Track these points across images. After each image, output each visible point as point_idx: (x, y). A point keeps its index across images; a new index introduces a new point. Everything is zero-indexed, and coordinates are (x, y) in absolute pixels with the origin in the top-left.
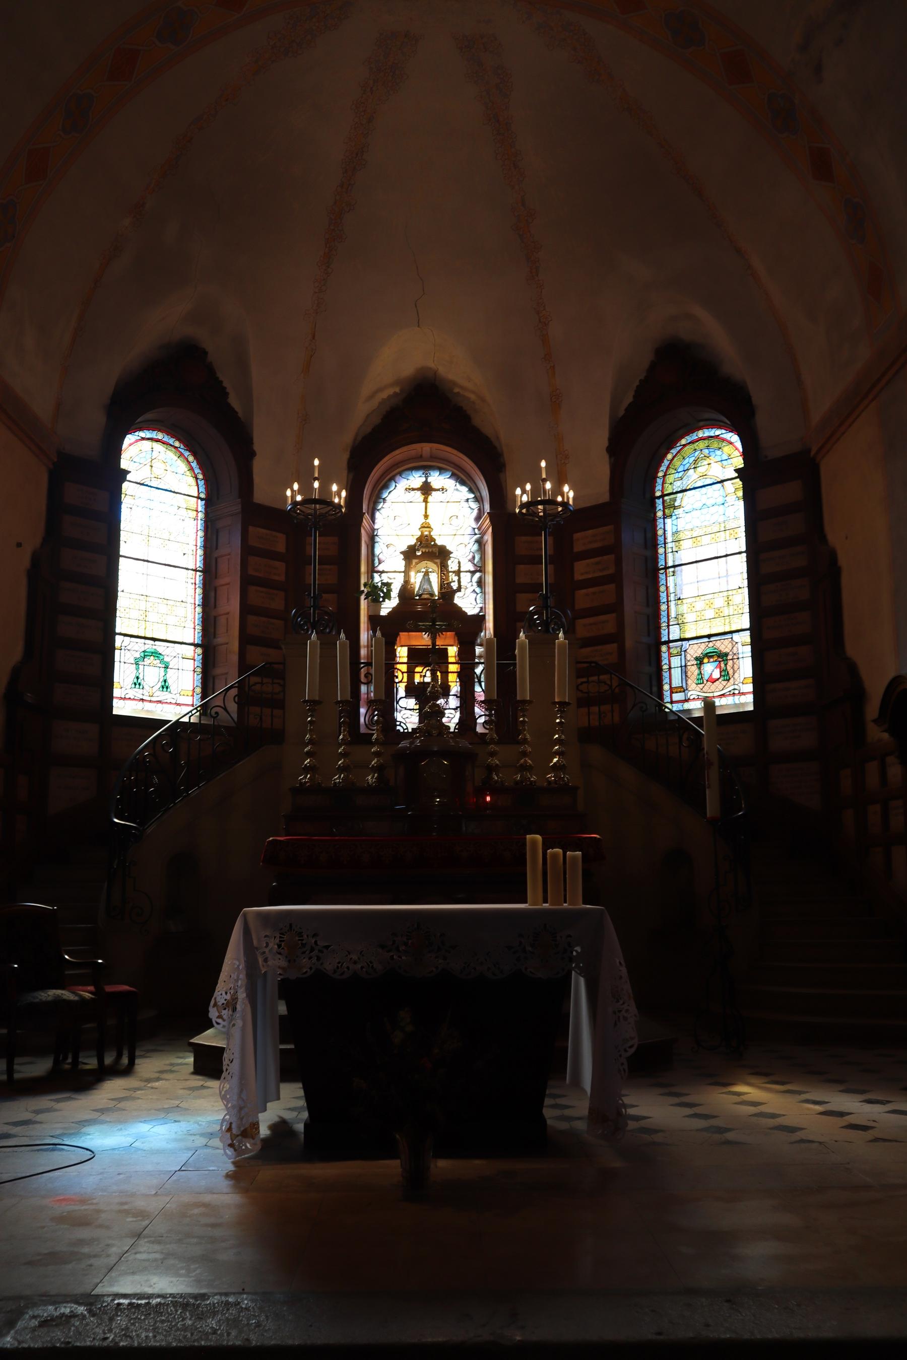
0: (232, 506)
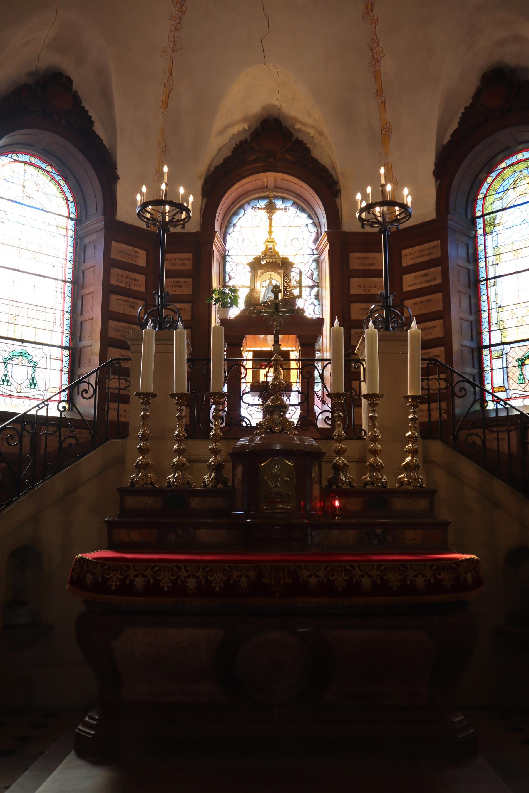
0: (97, 222)
